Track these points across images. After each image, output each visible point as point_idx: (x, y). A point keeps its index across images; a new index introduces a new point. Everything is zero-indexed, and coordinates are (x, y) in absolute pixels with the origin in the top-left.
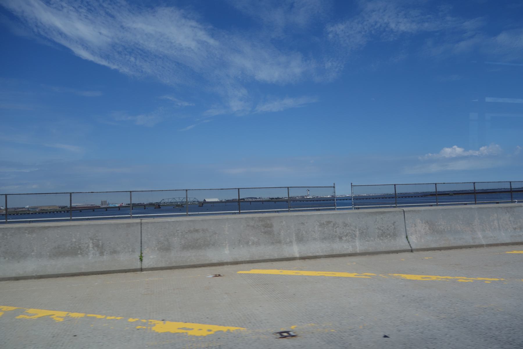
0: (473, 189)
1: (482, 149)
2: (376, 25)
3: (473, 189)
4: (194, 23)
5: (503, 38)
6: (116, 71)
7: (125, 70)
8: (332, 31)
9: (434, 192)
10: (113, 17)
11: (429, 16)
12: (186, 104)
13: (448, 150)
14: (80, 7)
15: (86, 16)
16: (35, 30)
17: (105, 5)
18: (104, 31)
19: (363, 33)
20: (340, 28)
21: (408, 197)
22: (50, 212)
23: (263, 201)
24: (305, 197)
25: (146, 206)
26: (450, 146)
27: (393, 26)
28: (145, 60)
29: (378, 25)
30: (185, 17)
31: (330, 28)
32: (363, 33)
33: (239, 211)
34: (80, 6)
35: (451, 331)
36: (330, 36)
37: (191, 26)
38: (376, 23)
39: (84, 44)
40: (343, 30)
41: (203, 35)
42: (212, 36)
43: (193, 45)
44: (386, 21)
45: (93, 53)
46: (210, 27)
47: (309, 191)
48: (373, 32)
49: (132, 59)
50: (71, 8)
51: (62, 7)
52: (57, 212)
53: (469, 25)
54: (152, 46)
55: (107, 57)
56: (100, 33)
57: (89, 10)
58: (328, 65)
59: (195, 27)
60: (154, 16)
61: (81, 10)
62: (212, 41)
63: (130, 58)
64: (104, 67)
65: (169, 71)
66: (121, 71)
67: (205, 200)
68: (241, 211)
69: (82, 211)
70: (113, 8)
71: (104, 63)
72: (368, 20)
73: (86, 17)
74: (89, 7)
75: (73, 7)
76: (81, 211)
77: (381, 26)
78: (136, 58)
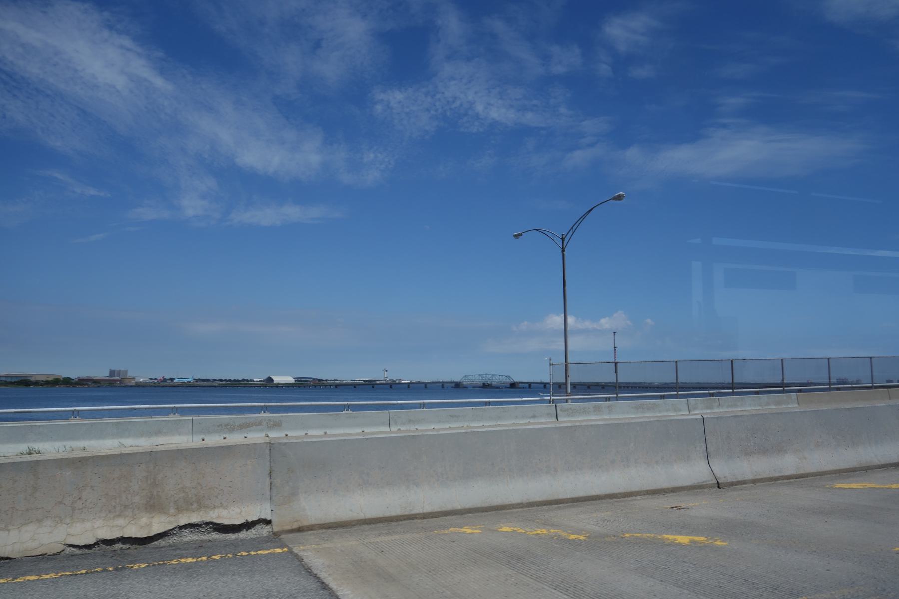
0: (731, 382)
1: (603, 321)
2: (454, 102)
3: (675, 382)
4: (127, 42)
5: (633, 154)
8: (382, 100)
9: (729, 384)
11: (535, 102)
12: (92, 192)
19: (432, 112)
20: (397, 97)
21: (649, 388)
23: (354, 385)
27: (480, 108)
28: (15, 96)
29: (458, 103)
30: (110, 28)
32: (432, 112)
33: (615, 395)
36: (379, 108)
37: (122, 47)
38: (455, 98)
40: (400, 102)
41: (141, 68)
42: (162, 72)
43: (121, 82)
44: (470, 98)
46: (160, 54)
47: (386, 371)
48: (448, 114)
53: (591, 126)
59: (129, 50)
60: (45, 12)
62: (159, 82)
65: (63, 123)
67: (270, 380)
68: (619, 395)
69: (357, 387)
72: (443, 93)
77: (461, 105)
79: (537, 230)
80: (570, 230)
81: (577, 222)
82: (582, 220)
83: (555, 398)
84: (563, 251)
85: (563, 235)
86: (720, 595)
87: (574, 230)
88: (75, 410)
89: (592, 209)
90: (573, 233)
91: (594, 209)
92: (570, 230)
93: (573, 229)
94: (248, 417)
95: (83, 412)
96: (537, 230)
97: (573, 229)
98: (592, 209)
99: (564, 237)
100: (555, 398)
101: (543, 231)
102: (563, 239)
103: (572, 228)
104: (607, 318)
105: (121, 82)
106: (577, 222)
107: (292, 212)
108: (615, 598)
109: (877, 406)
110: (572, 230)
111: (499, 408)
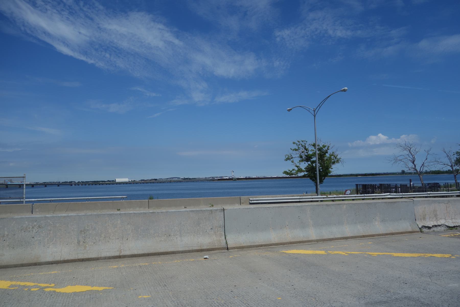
4: (161, 26)
5: (424, 44)
7: (101, 64)
10: (92, 19)
13: (373, 138)
14: (62, 10)
15: (67, 18)
16: (22, 28)
18: (83, 31)
20: (286, 33)
25: (8, 186)
27: (331, 32)
30: (154, 21)
34: (63, 10)
36: (278, 39)
37: (159, 29)
39: (65, 42)
40: (288, 35)
41: (169, 36)
42: (177, 37)
43: (161, 44)
46: (176, 29)
49: (107, 55)
50: (55, 11)
51: (47, 10)
54: (124, 44)
55: (85, 53)
56: (80, 33)
57: (71, 13)
61: (63, 13)
62: (176, 42)
63: (105, 55)
64: (82, 61)
69: (60, 185)
70: (92, 12)
71: (83, 58)
73: (68, 19)
74: (71, 10)
75: (57, 10)
76: (59, 186)
78: (110, 55)
79: (300, 106)
80: (318, 106)
82: (326, 100)
83: (26, 200)
84: (315, 116)
86: (247, 271)
87: (320, 106)
88: (51, 200)
89: (330, 95)
90: (320, 108)
91: (330, 96)
92: (318, 106)
93: (320, 106)
95: (116, 199)
97: (320, 106)
98: (330, 95)
99: (315, 109)
100: (26, 200)
101: (303, 107)
102: (314, 111)
105: (161, 44)
107: (244, 95)
108: (393, 306)
111: (236, 198)
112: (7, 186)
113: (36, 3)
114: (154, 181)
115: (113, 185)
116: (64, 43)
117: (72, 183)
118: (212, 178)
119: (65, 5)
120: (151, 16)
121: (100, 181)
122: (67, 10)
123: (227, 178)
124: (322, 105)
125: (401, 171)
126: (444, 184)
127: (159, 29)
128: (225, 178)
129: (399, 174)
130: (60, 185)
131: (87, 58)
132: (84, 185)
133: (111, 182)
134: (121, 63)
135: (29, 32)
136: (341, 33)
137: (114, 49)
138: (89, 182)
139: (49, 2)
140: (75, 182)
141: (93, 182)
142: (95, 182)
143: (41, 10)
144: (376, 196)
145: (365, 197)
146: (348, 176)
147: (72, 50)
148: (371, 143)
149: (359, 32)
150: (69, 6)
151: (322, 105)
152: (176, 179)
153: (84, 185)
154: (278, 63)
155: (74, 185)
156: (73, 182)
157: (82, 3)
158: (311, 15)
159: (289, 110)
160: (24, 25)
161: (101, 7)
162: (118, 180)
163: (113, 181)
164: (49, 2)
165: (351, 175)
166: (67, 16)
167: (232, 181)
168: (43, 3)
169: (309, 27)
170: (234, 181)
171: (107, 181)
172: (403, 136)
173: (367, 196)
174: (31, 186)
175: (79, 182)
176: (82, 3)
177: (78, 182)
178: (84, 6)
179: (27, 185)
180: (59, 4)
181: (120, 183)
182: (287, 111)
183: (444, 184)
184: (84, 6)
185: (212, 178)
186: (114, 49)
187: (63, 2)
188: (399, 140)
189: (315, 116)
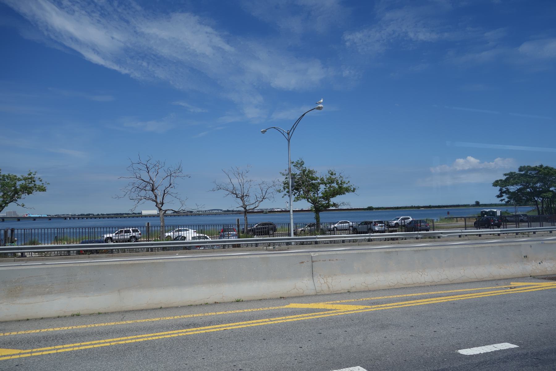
4: (209, 30)
5: (526, 48)
6: (127, 76)
7: (136, 75)
10: (128, 22)
13: (461, 161)
14: (93, 12)
15: (98, 20)
16: (46, 33)
17: (119, 10)
18: (117, 36)
20: (358, 36)
22: (70, 218)
24: (497, 227)
25: (5, 219)
26: (464, 157)
27: (411, 35)
28: (158, 65)
30: (200, 23)
31: (331, 199)
34: (93, 11)
35: (323, 201)
36: (348, 44)
37: (207, 33)
39: (95, 49)
41: (218, 41)
42: (228, 42)
43: (209, 51)
45: (104, 58)
48: (391, 41)
49: (145, 64)
50: (84, 12)
51: (74, 11)
52: (70, 218)
54: (165, 51)
55: (118, 61)
56: (113, 38)
57: (102, 15)
58: (346, 73)
61: (93, 15)
62: (227, 48)
63: (142, 63)
64: (115, 71)
66: (132, 76)
69: (52, 219)
70: (128, 13)
71: (116, 68)
73: (99, 21)
74: (102, 11)
75: (86, 12)
76: (50, 219)
78: (148, 63)
79: (274, 128)
80: (292, 128)
81: (295, 123)
84: (289, 141)
85: (288, 131)
90: (294, 130)
91: (305, 114)
92: (292, 128)
94: (57, 267)
96: (274, 128)
98: (305, 113)
99: (289, 132)
101: (278, 129)
102: (288, 134)
103: (293, 126)
104: (478, 161)
106: (295, 123)
109: (60, 353)
110: (293, 128)
112: (4, 219)
113: (62, 4)
114: (189, 214)
115: (125, 218)
116: (94, 50)
117: (90, 215)
118: (260, 210)
119: (96, 5)
120: (197, 17)
121: (124, 214)
122: (99, 11)
123: (279, 210)
124: (297, 124)
125: (474, 203)
126: (6, 232)
127: (207, 33)
128: (277, 210)
129: (473, 206)
130: (52, 219)
131: (120, 67)
132: (81, 218)
133: (137, 214)
134: (161, 74)
135: (53, 37)
136: (424, 36)
137: (152, 56)
138: (110, 214)
139: (78, 3)
140: (93, 214)
141: (115, 214)
142: (117, 214)
143: (67, 12)
144: (482, 232)
145: (462, 233)
146: (408, 209)
147: (103, 59)
148: (458, 168)
149: (446, 35)
150: (101, 7)
151: (297, 124)
152: (216, 211)
153: (81, 218)
154: (348, 72)
155: (68, 219)
156: (91, 214)
157: (116, 4)
158: (388, 15)
159: (264, 132)
160: (47, 30)
161: (138, 8)
162: (144, 213)
163: (139, 213)
164: (78, 3)
165: (412, 207)
166: (98, 18)
167: (262, 214)
168: (69, 4)
169: (385, 29)
170: (265, 214)
171: (132, 214)
172: (498, 160)
173: (373, 235)
174: (16, 220)
175: (98, 215)
176: (116, 4)
177: (97, 215)
178: (118, 6)
179: (293, 211)
180: (89, 4)
181: (146, 216)
182: (261, 133)
183: (6, 232)
184: (118, 6)
185: (260, 210)
186: (152, 56)
187: (93, 2)
188: (491, 163)
189: (289, 141)
